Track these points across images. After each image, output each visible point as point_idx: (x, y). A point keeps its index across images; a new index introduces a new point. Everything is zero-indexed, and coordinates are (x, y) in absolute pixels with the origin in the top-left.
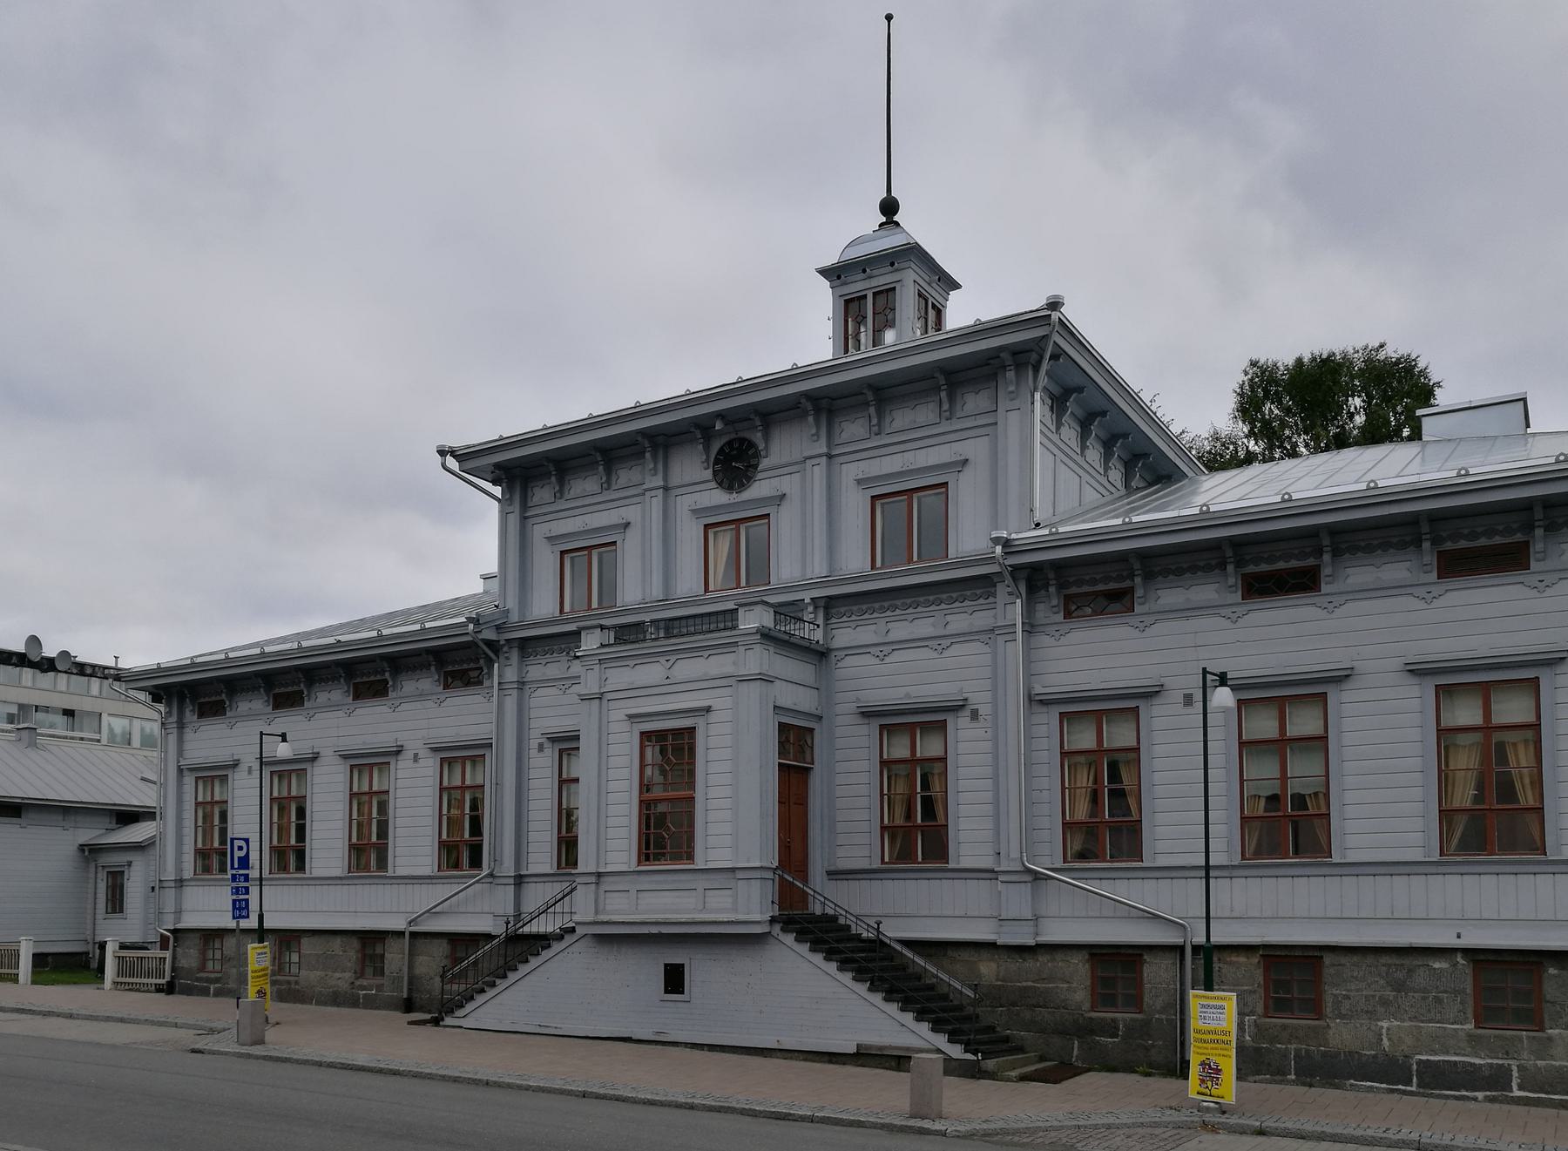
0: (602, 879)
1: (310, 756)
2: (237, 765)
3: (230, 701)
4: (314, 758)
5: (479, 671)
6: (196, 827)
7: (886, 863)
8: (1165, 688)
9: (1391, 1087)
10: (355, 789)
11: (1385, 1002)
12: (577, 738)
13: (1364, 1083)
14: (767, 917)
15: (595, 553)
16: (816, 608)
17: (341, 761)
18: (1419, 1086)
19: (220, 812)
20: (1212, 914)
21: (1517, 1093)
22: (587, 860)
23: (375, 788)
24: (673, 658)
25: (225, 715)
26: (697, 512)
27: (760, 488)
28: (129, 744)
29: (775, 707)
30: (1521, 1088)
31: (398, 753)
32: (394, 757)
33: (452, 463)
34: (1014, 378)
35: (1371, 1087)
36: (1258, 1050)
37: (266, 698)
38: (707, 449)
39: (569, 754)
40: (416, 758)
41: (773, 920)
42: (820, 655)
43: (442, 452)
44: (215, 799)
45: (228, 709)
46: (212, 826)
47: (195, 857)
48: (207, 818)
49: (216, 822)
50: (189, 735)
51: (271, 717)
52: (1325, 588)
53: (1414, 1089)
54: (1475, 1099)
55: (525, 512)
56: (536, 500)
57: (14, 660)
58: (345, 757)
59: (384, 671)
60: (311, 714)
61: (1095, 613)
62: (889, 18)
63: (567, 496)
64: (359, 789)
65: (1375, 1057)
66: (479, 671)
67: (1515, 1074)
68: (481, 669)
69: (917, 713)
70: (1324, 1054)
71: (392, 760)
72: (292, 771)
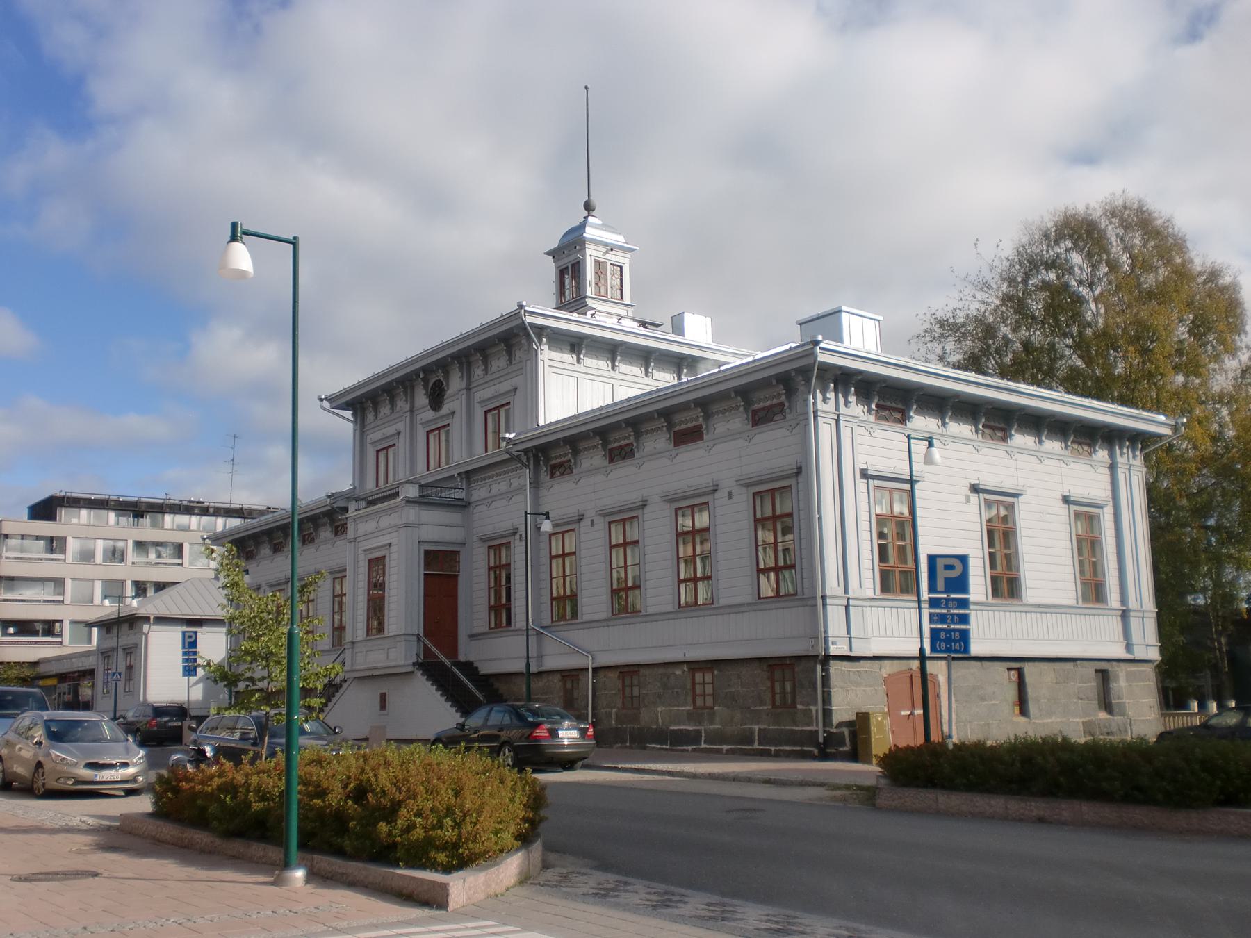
0: (356, 645)
1: (712, 488)
2: (716, 490)
3: (789, 402)
4: (644, 505)
5: (782, 407)
6: (489, 588)
7: (492, 628)
8: (648, 503)
9: (712, 746)
10: (759, 516)
11: (660, 697)
12: (345, 570)
13: (782, 748)
14: (411, 662)
15: (502, 411)
16: (462, 479)
17: (744, 490)
18: (671, 745)
19: (506, 575)
20: (530, 655)
21: (703, 746)
22: (348, 636)
23: (779, 512)
24: (378, 516)
25: (703, 439)
26: (424, 424)
27: (445, 410)
28: (92, 602)
29: (419, 542)
30: (760, 744)
31: (580, 520)
32: (641, 510)
33: (326, 404)
34: (526, 344)
35: (654, 747)
36: (617, 728)
37: (745, 416)
38: (425, 387)
39: (781, 493)
40: (730, 495)
41: (414, 664)
42: (463, 506)
43: (321, 400)
44: (627, 541)
45: (787, 411)
46: (501, 586)
47: (612, 596)
48: (497, 579)
49: (504, 582)
50: (543, 492)
51: (674, 453)
52: (636, 455)
53: (668, 747)
54: (687, 751)
55: (364, 428)
56: (382, 414)
57: (211, 510)
58: (748, 486)
59: (779, 395)
60: (510, 496)
61: (562, 474)
62: (586, 88)
63: (489, 373)
64: (762, 515)
65: (656, 729)
66: (782, 407)
67: (703, 735)
68: (632, 444)
69: (762, 483)
70: (639, 729)
71: (639, 513)
72: (624, 517)
